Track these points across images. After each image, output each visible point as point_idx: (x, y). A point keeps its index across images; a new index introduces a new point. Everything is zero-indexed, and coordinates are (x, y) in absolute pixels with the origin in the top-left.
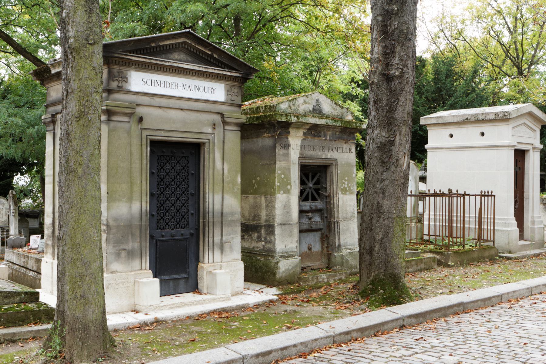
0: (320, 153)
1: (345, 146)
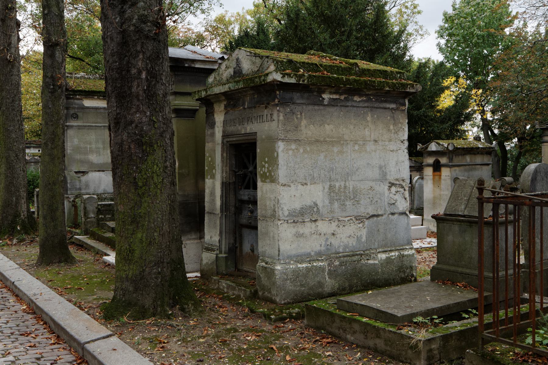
0: (239, 128)
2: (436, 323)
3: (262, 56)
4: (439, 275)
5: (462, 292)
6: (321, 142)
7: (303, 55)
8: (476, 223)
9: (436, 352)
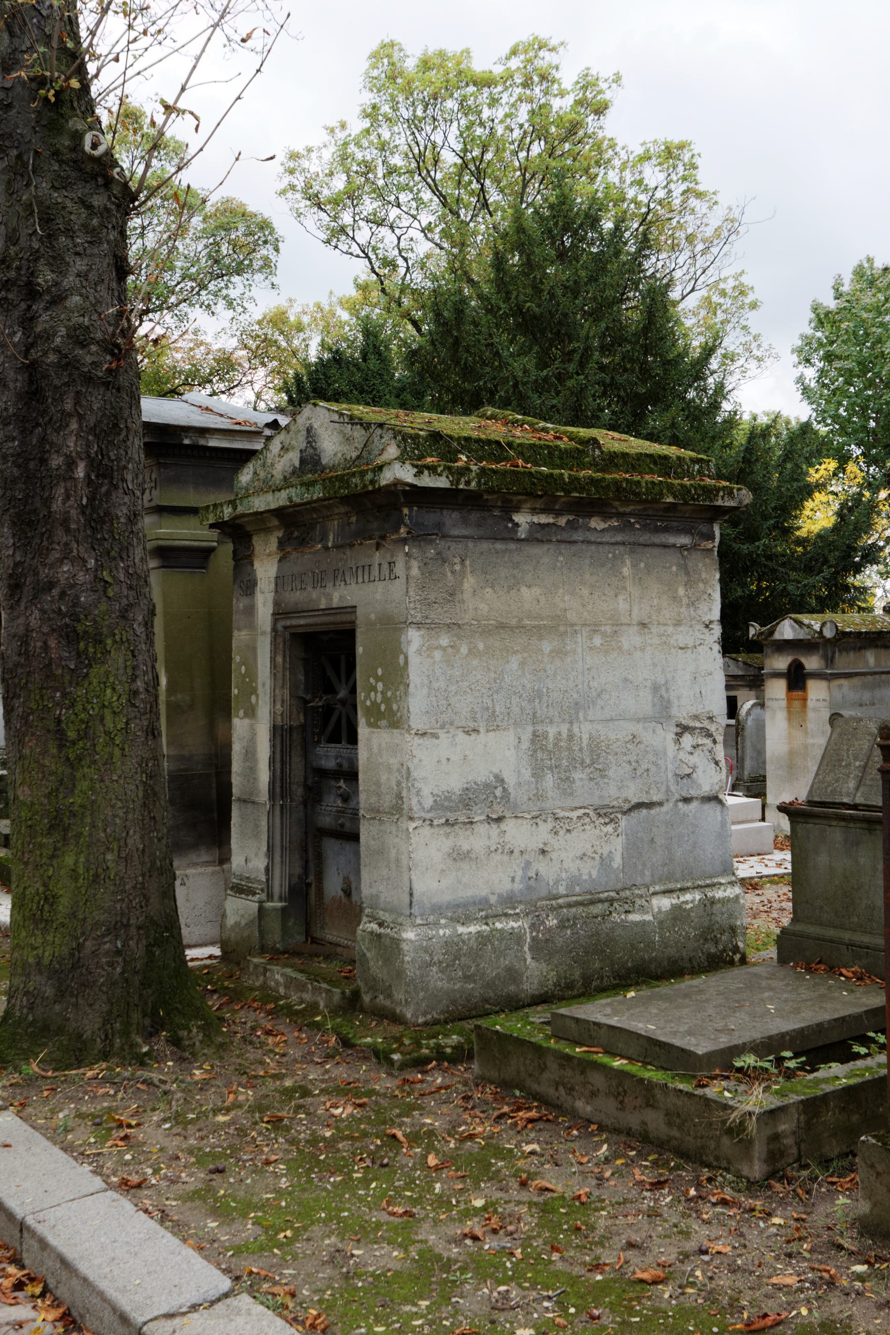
0: (314, 595)
1: (377, 557)
2: (788, 1068)
3: (369, 424)
4: (793, 949)
5: (852, 991)
6: (512, 628)
7: (467, 419)
8: (879, 821)
9: (789, 1141)
